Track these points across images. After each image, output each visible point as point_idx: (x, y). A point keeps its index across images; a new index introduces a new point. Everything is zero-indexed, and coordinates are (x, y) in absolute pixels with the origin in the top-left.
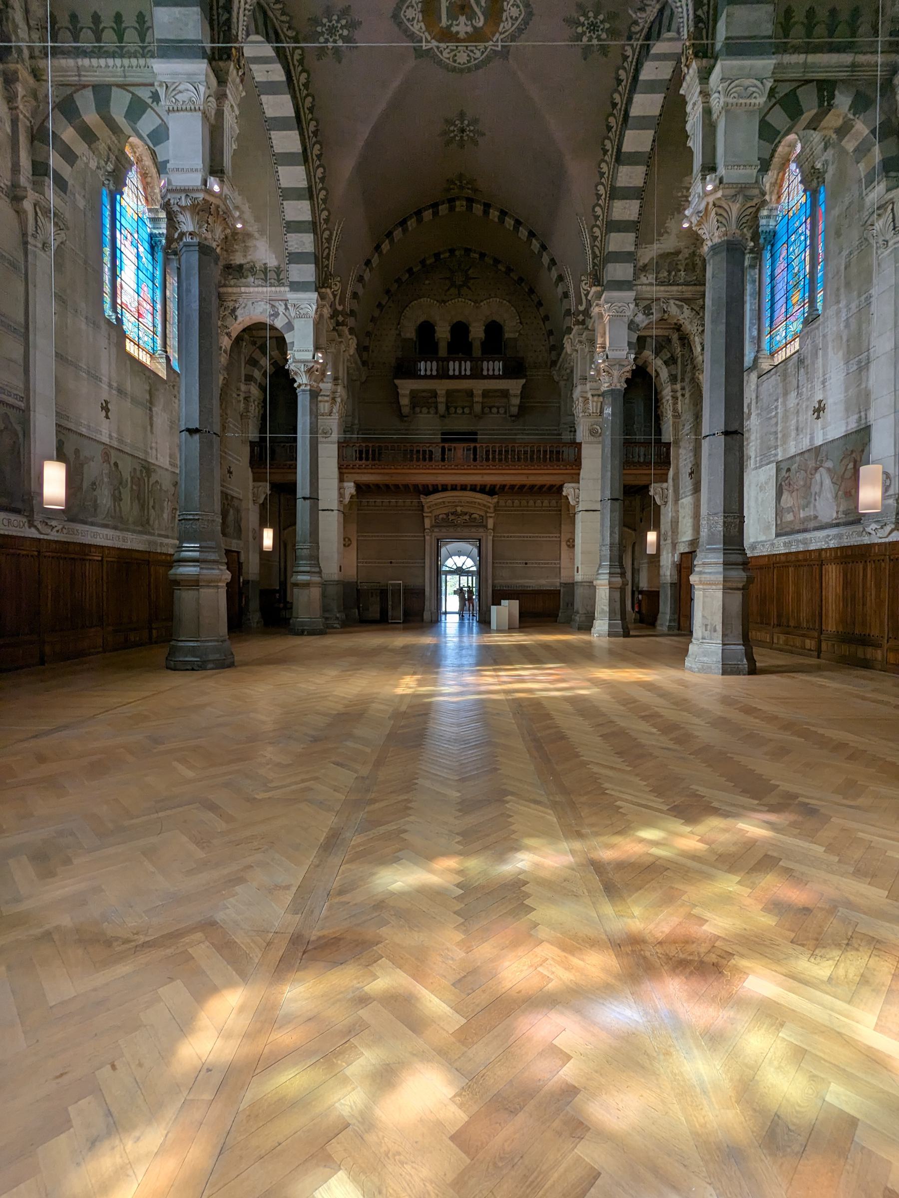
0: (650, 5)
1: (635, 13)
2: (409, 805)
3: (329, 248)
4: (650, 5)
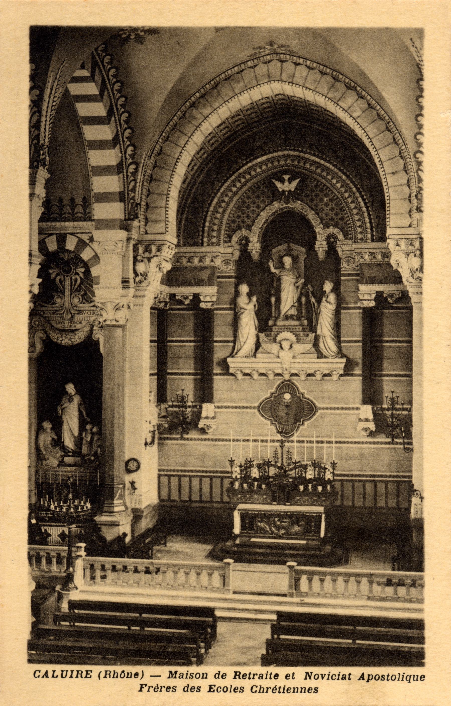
2: (63, 407)
3: (135, 180)
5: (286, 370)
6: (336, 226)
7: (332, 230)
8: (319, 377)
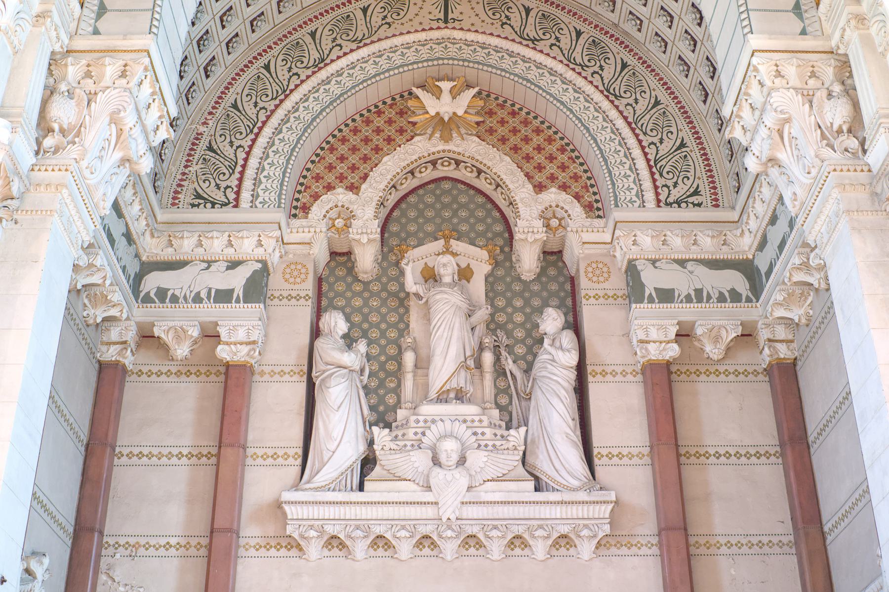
5: (449, 527)
6: (564, 187)
7: (552, 196)
8: (540, 548)
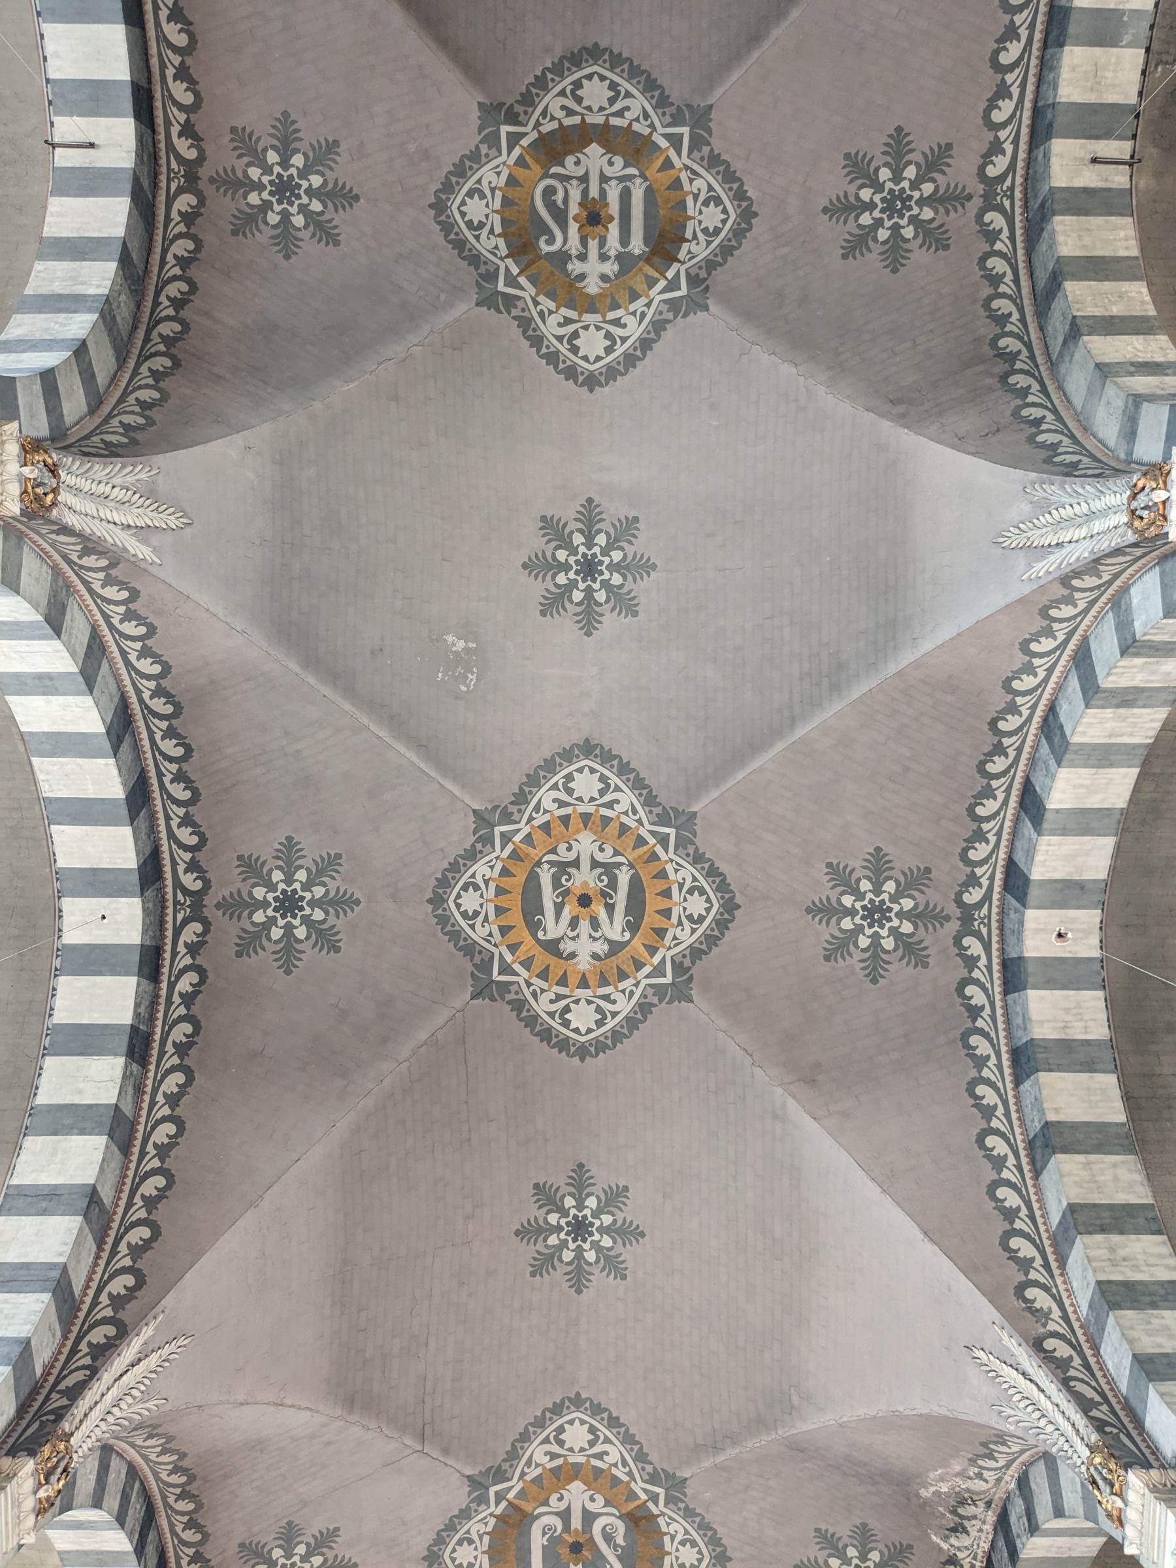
0: (975, 1517)
1: (946, 1538)
4: (975, 1517)
